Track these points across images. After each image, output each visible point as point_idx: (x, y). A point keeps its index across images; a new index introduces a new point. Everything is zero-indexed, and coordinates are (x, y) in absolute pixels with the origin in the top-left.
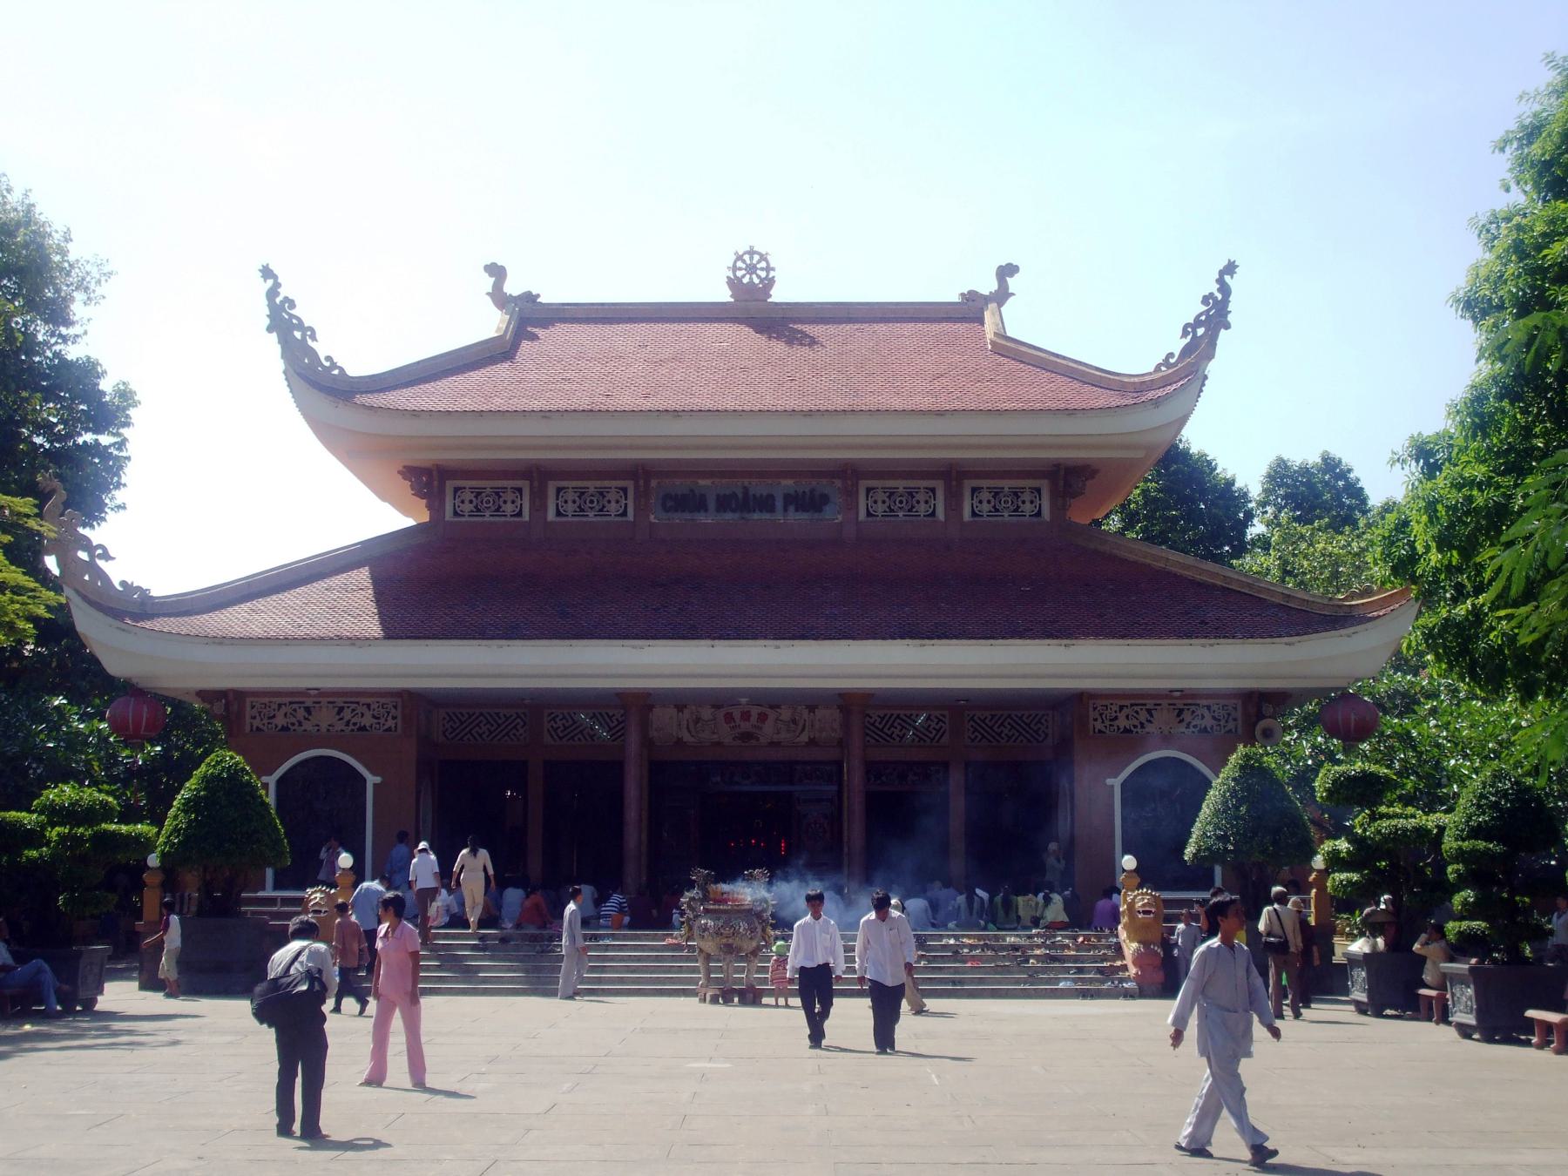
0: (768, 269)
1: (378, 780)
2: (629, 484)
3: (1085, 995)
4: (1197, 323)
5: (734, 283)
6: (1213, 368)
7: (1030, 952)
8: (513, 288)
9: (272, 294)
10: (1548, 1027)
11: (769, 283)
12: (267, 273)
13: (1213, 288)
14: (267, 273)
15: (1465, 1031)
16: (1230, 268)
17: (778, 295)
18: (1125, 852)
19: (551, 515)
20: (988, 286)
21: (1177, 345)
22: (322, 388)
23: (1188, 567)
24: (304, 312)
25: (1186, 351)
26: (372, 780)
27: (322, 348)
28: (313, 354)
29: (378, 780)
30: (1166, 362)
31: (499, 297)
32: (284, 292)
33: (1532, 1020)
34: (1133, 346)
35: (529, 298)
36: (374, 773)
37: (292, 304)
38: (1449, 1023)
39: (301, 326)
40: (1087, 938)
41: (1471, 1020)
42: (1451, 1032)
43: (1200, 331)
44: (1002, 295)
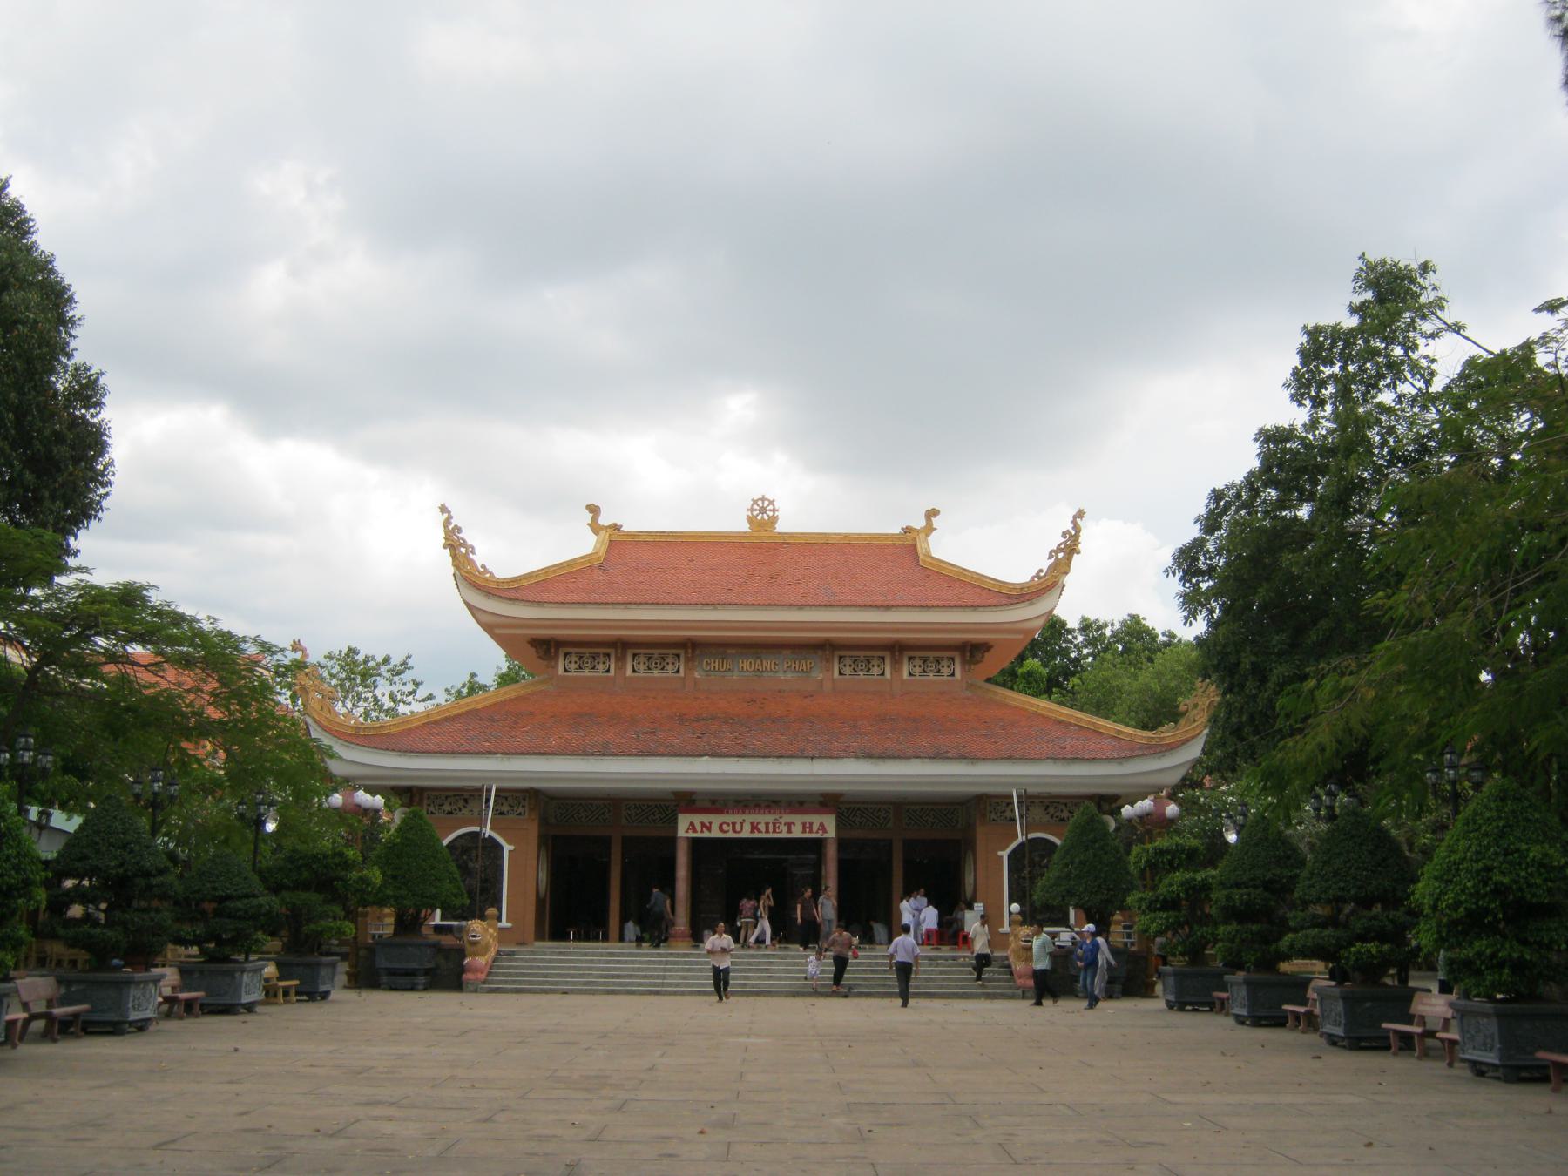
0: (774, 510)
1: (512, 848)
2: (681, 652)
3: (989, 996)
4: (1059, 550)
5: (751, 520)
6: (1068, 580)
7: (1342, 917)
8: (604, 521)
9: (447, 523)
10: (1297, 1016)
11: (774, 520)
12: (443, 509)
13: (1070, 527)
14: (443, 509)
15: (1241, 1021)
16: (1080, 514)
17: (782, 527)
18: (1011, 901)
19: (629, 672)
20: (919, 523)
21: (1045, 564)
22: (469, 576)
23: (1050, 710)
24: (468, 535)
25: (1052, 568)
26: (508, 848)
27: (479, 559)
28: (472, 562)
29: (512, 848)
30: (1037, 575)
31: (595, 527)
32: (454, 522)
33: (1388, 1030)
34: (1015, 564)
35: (616, 527)
36: (509, 843)
37: (460, 530)
38: (1227, 1014)
39: (464, 544)
40: (34, 274)
41: (1339, 1031)
42: (1231, 1021)
43: (1061, 555)
44: (929, 529)
